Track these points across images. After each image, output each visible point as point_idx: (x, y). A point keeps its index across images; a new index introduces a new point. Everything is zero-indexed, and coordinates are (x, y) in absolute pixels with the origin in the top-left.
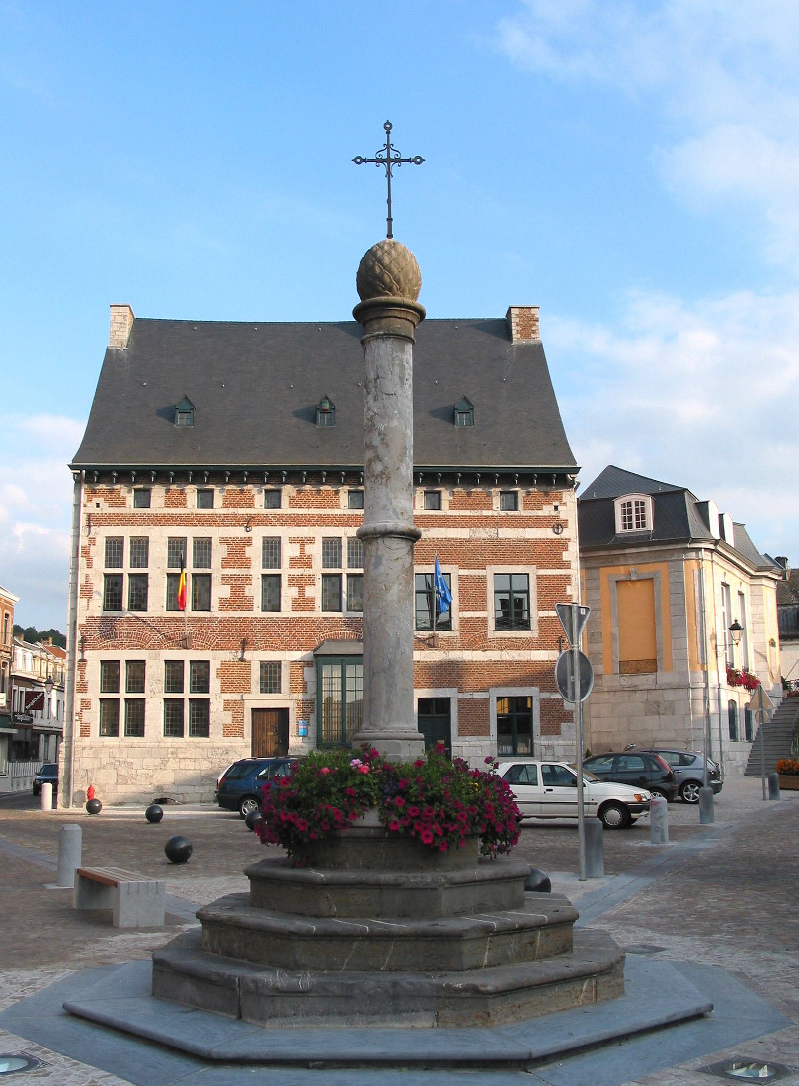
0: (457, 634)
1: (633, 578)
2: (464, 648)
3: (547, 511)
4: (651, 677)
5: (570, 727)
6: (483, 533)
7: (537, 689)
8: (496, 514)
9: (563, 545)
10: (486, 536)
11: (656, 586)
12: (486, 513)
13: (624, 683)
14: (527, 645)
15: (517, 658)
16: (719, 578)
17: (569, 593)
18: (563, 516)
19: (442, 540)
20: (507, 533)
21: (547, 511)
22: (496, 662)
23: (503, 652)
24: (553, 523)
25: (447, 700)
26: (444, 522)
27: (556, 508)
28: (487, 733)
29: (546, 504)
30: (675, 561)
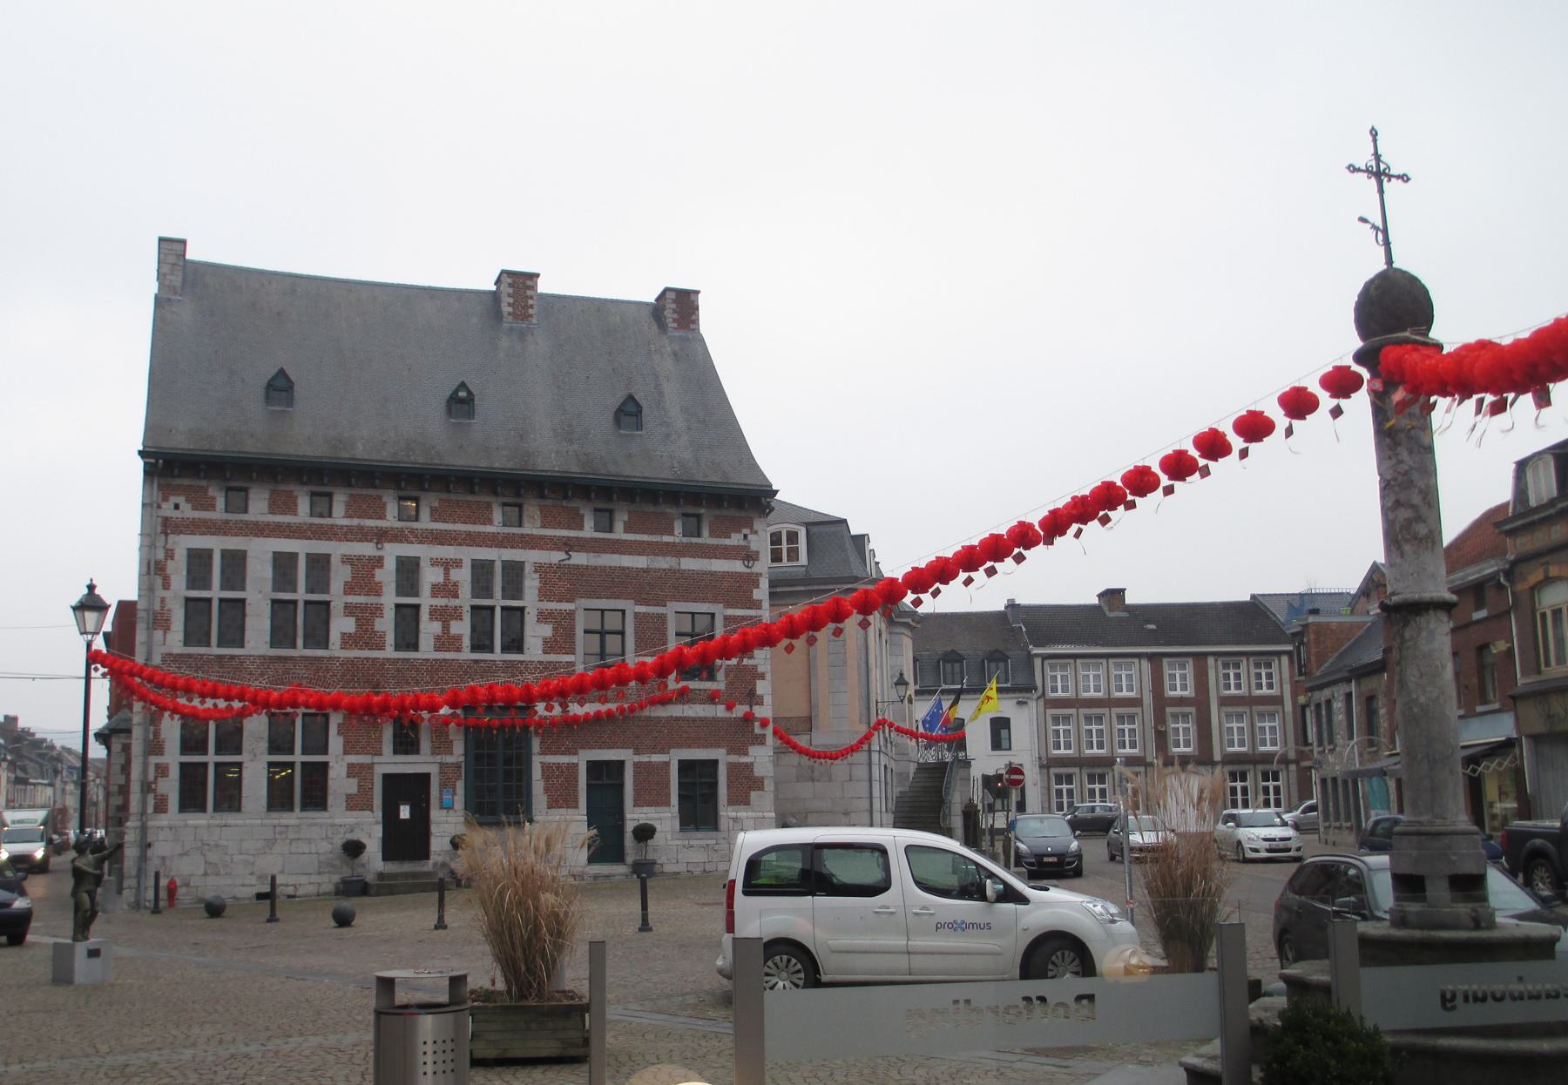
6: (663, 563)
9: (753, 581)
12: (666, 539)
15: (702, 714)
21: (735, 540)
25: (621, 763)
27: (745, 536)
28: (668, 804)
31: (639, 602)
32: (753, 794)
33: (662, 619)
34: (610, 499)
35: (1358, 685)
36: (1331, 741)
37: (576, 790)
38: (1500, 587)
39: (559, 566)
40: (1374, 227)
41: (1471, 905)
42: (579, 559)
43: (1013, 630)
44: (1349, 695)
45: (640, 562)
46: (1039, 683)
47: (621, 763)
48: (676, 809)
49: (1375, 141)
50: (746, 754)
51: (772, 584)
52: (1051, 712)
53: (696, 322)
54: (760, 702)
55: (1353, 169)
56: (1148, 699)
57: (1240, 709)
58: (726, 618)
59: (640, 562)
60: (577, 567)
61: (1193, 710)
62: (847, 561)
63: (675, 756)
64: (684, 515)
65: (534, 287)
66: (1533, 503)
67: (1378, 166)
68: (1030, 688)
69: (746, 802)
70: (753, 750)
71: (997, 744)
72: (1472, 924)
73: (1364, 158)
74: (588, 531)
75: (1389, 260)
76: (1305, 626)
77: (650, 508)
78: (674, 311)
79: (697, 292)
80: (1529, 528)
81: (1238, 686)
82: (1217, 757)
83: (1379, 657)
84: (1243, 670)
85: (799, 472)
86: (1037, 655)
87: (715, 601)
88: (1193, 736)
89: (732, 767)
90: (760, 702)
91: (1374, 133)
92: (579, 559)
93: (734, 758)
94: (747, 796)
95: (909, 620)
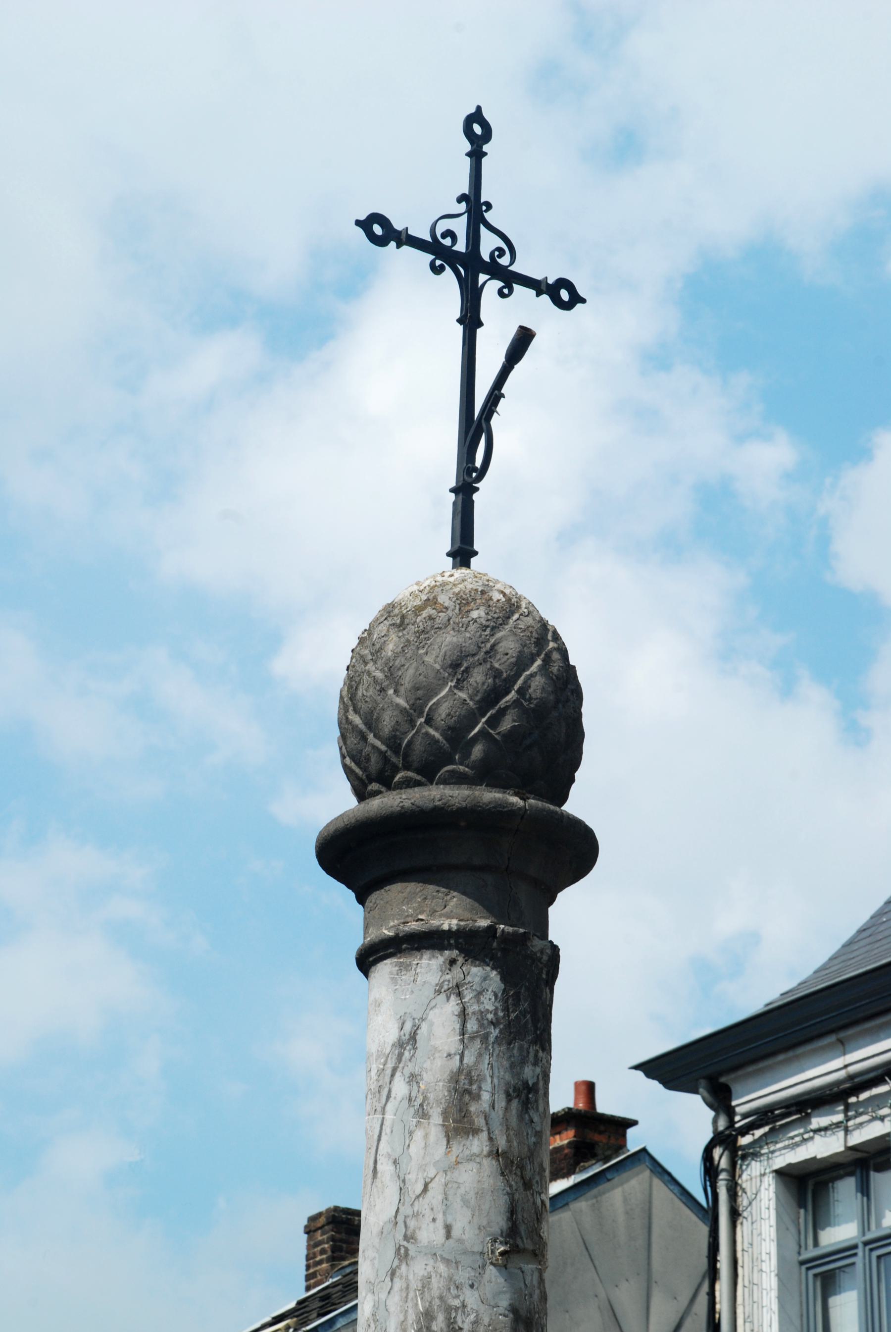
49: (476, 156)
73: (427, 200)
91: (477, 131)
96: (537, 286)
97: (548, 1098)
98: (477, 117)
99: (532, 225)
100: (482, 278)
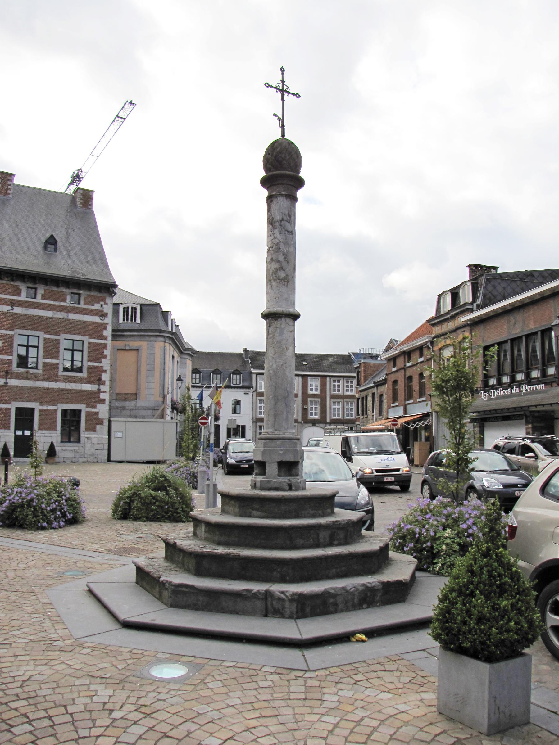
0: (41, 371)
1: (127, 348)
2: (44, 379)
3: (97, 307)
4: (134, 403)
5: (101, 428)
6: (60, 315)
7: (84, 406)
8: (68, 305)
9: (104, 326)
10: (61, 317)
11: (140, 354)
12: (62, 304)
13: (118, 405)
14: (81, 381)
15: (75, 388)
16: (171, 353)
17: (105, 353)
18: (105, 311)
19: (36, 316)
20: (73, 316)
21: (97, 307)
22: (63, 390)
23: (67, 384)
24: (100, 314)
25: (33, 409)
26: (37, 306)
27: (102, 306)
28: (55, 429)
29: (96, 303)
30: (151, 341)
31: (46, 333)
32: (98, 427)
33: (58, 341)
34: (35, 283)
35: (377, 389)
36: (366, 414)
37: (9, 421)
38: (429, 348)
39: (7, 313)
40: (279, 119)
41: (289, 478)
42: (18, 310)
43: (245, 361)
44: (373, 394)
45: (49, 314)
46: (254, 385)
47: (33, 409)
48: (59, 432)
49: (282, 74)
50: (95, 407)
51: (113, 330)
52: (259, 398)
53: (91, 205)
54: (104, 383)
55: (267, 85)
56: (300, 394)
57: (339, 400)
58: (89, 343)
59: (49, 314)
60: (16, 314)
61: (319, 400)
62: (158, 323)
63: (60, 407)
64: (72, 293)
65: (11, 180)
66: (442, 313)
67: (283, 87)
68: (250, 387)
69: (95, 430)
70: (99, 406)
71: (234, 411)
72: (287, 488)
73: (275, 81)
74: (23, 297)
75: (283, 135)
76: (360, 364)
77: (55, 289)
78: (81, 199)
79: (93, 191)
80: (440, 323)
81: (339, 390)
82: (328, 420)
83: (384, 378)
84: (341, 384)
85: (132, 279)
86: (254, 373)
87: (84, 335)
88: (318, 411)
89: (88, 413)
90: (104, 383)
91: (282, 70)
92: (18, 310)
93: (89, 409)
94: (95, 427)
95: (190, 352)
96: (294, 94)
97: (324, 357)
98: (282, 68)
99: (292, 86)
100: (285, 93)
